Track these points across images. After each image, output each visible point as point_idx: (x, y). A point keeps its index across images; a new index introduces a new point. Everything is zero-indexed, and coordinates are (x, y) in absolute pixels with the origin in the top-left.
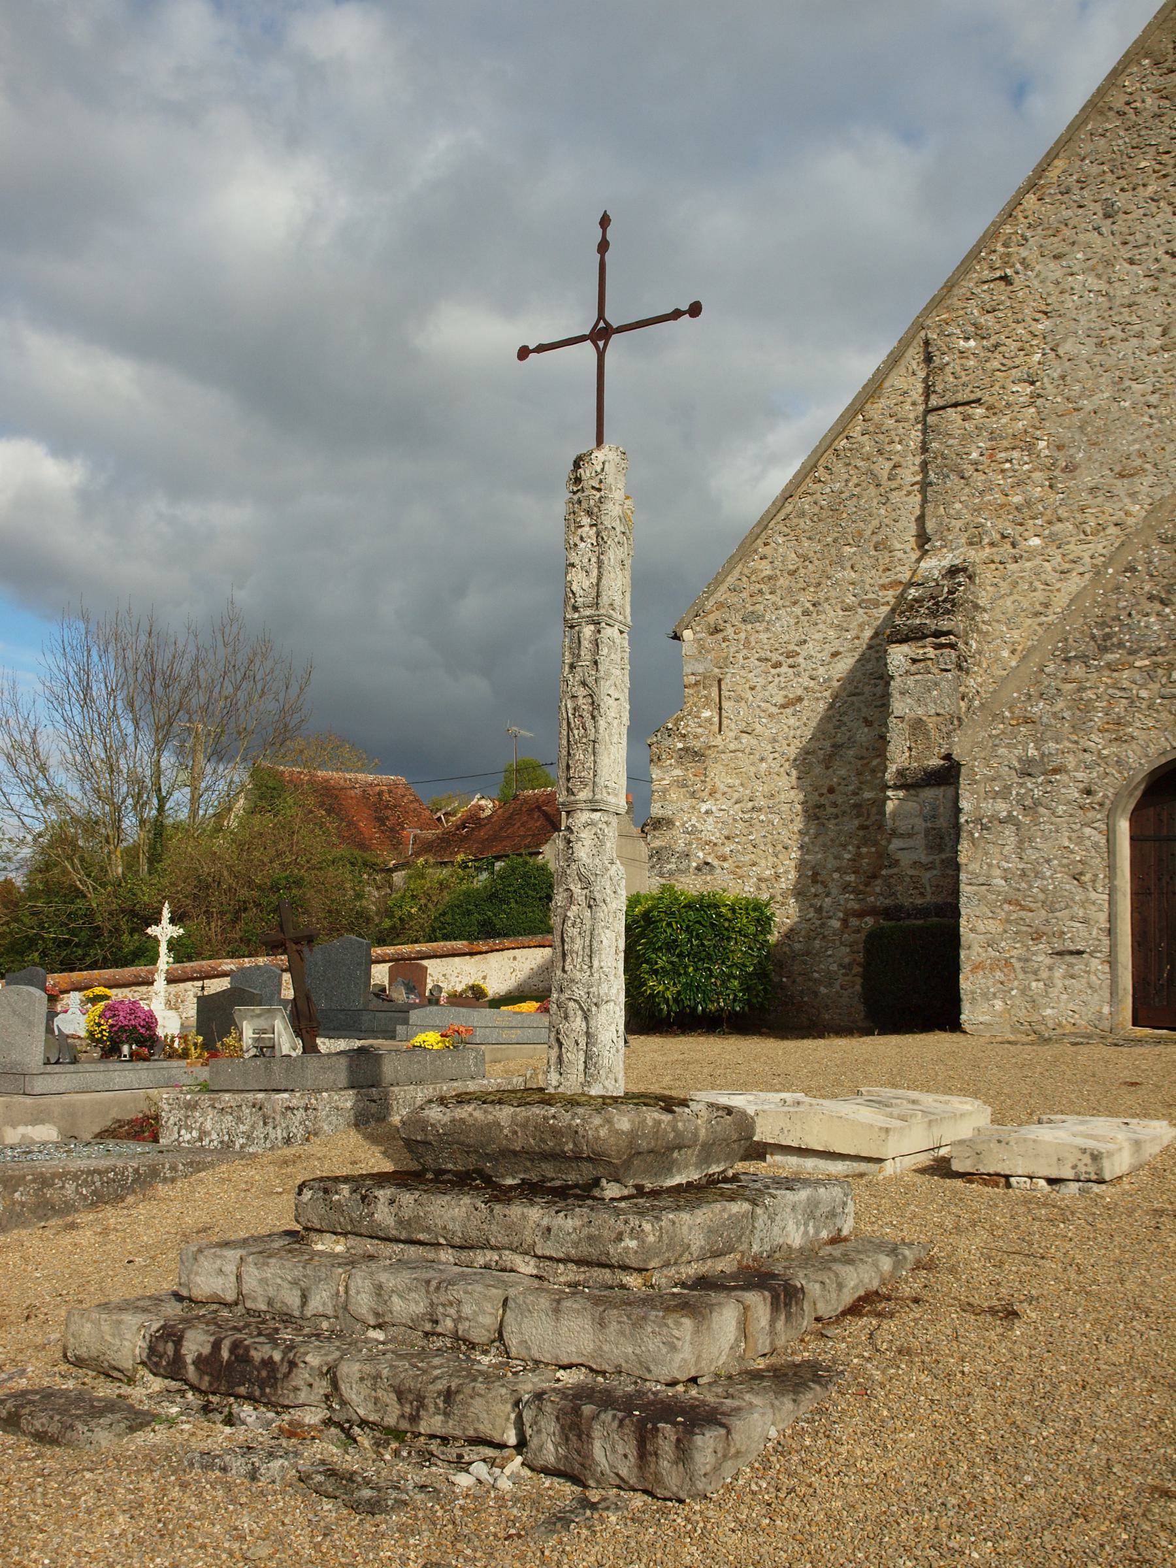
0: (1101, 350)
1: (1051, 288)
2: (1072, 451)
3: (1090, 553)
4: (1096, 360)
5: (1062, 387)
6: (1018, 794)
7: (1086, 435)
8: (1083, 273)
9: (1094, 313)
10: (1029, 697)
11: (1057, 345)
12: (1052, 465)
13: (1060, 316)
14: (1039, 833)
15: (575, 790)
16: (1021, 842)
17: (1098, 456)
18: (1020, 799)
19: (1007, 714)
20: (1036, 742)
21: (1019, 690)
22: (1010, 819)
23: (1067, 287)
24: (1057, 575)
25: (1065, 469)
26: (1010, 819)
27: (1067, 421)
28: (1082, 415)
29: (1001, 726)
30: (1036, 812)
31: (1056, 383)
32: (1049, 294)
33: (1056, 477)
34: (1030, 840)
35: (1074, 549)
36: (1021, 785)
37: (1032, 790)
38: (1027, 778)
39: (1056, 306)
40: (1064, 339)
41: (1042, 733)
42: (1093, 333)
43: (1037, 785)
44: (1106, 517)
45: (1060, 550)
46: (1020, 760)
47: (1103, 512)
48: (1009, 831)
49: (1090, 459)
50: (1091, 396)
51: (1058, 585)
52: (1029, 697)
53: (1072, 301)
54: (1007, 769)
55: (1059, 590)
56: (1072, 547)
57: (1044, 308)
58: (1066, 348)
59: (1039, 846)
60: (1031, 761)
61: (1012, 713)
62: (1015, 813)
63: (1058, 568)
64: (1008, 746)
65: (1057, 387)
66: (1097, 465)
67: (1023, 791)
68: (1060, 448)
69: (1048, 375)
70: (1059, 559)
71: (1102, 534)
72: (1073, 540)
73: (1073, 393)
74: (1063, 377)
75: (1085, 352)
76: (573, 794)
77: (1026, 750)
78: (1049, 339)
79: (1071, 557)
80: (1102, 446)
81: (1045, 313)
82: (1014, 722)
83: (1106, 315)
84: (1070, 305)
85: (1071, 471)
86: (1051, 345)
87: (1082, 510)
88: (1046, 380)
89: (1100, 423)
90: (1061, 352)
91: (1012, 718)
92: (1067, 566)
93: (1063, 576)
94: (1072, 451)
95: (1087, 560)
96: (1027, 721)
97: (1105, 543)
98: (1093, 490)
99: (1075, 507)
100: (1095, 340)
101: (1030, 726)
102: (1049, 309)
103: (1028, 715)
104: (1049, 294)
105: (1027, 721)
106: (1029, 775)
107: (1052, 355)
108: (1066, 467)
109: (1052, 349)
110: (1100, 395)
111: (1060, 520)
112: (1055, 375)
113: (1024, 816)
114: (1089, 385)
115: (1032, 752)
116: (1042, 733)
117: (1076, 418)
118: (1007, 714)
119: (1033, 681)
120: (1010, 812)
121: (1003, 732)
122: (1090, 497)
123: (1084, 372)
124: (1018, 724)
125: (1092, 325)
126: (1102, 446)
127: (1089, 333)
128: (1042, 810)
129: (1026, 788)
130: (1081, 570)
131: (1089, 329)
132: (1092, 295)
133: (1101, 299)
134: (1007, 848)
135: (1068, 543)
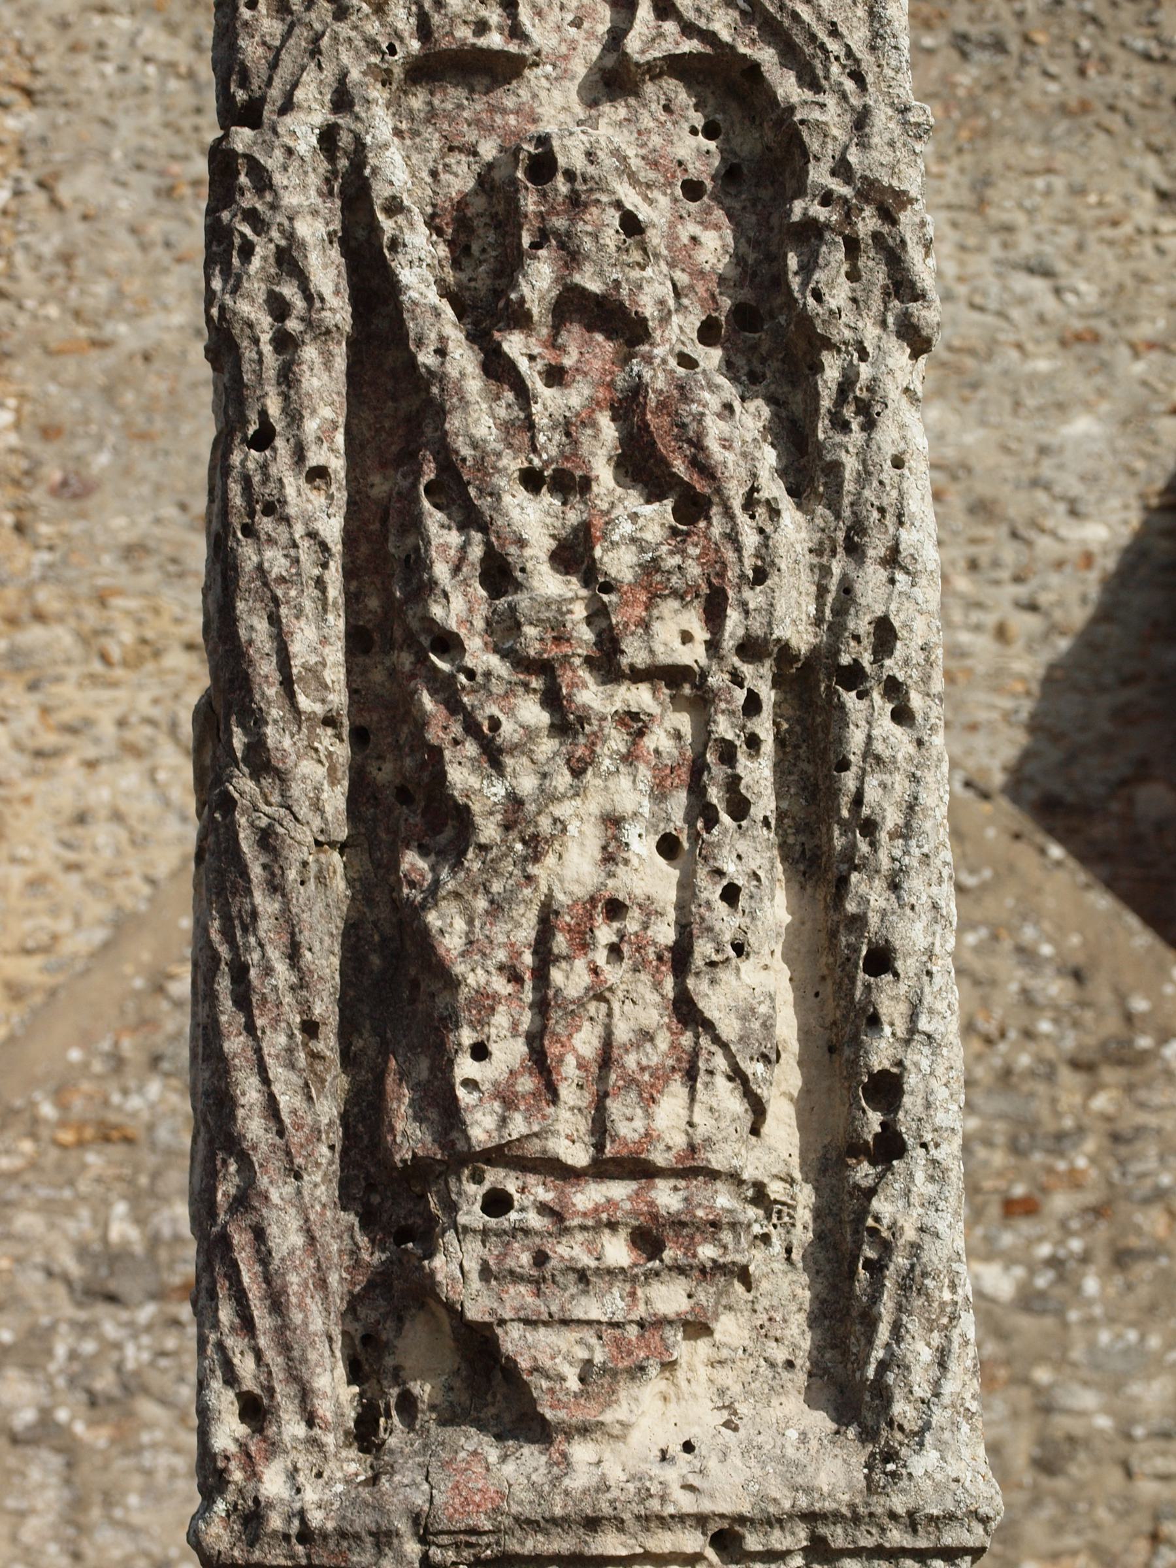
0: (168, 207)
1: (47, 33)
2: (80, 446)
3: (117, 711)
4: (155, 229)
5: (60, 282)
6: (73, 1355)
7: (121, 410)
8: (133, 13)
9: (154, 116)
10: (118, 1062)
11: (56, 176)
12: (27, 473)
13: (66, 105)
14: (137, 1480)
15: (558, 1389)
16: (78, 1504)
17: (149, 468)
18: (79, 1374)
19: (48, 1110)
20: (135, 1199)
21: (86, 1040)
22: (45, 1431)
23: (89, 38)
24: (24, 761)
25: (61, 489)
26: (45, 1431)
27: (70, 368)
28: (110, 358)
29: (27, 1146)
30: (130, 1414)
31: (46, 269)
32: (40, 48)
33: (33, 508)
34: (109, 1500)
35: (72, 697)
36: (84, 1329)
37: (118, 1346)
38: (102, 1310)
39: (59, 80)
40: (76, 163)
41: (155, 1175)
42: (151, 163)
43: (135, 1330)
44: (165, 624)
45: (37, 697)
46: (82, 1252)
47: (157, 611)
48: (42, 1470)
49: (127, 472)
50: (137, 315)
51: (26, 787)
52: (118, 1062)
53: (96, 77)
54: (38, 1277)
55: (27, 800)
56: (67, 690)
57: (24, 78)
58: (82, 186)
59: (137, 1519)
60: (115, 1257)
61: (63, 1106)
62: (62, 1415)
63: (30, 743)
64: (47, 1207)
65: (50, 279)
66: (145, 489)
67: (89, 1347)
68: (49, 432)
69: (27, 247)
70: (31, 717)
71: (150, 666)
72: (73, 673)
73: (90, 302)
74: (66, 258)
75: (126, 204)
76: (494, 1392)
77: (103, 1224)
78: (35, 157)
79: (66, 716)
80: (161, 443)
81: (28, 93)
82: (67, 1137)
83: (187, 123)
84: (96, 84)
85: (76, 496)
86: (42, 172)
87: (101, 599)
88: (19, 258)
89: (157, 385)
90: (64, 192)
91: (63, 1124)
92: (49, 739)
93: (40, 764)
94: (80, 446)
95: (107, 728)
96: (108, 1134)
97: (156, 691)
98: (133, 552)
99: (83, 589)
100: (154, 181)
101: (118, 1151)
102: (38, 84)
103: (113, 1117)
104: (40, 48)
105: (108, 1134)
106: (112, 1298)
107: (39, 199)
108: (65, 483)
109: (41, 184)
110: (160, 317)
111: (39, 617)
112: (47, 249)
113: (91, 1424)
114: (134, 287)
115: (122, 1228)
116: (155, 1175)
117: (97, 365)
118: (48, 1110)
119: (132, 1018)
120: (46, 1414)
121: (33, 1165)
122: (123, 568)
123: (121, 253)
124: (81, 1144)
125: (150, 143)
126: (161, 443)
127: (142, 159)
128: (148, 1408)
129: (101, 1338)
130: (91, 753)
131: (141, 150)
132: (151, 69)
133: (173, 84)
134: (33, 1523)
135: (59, 679)
